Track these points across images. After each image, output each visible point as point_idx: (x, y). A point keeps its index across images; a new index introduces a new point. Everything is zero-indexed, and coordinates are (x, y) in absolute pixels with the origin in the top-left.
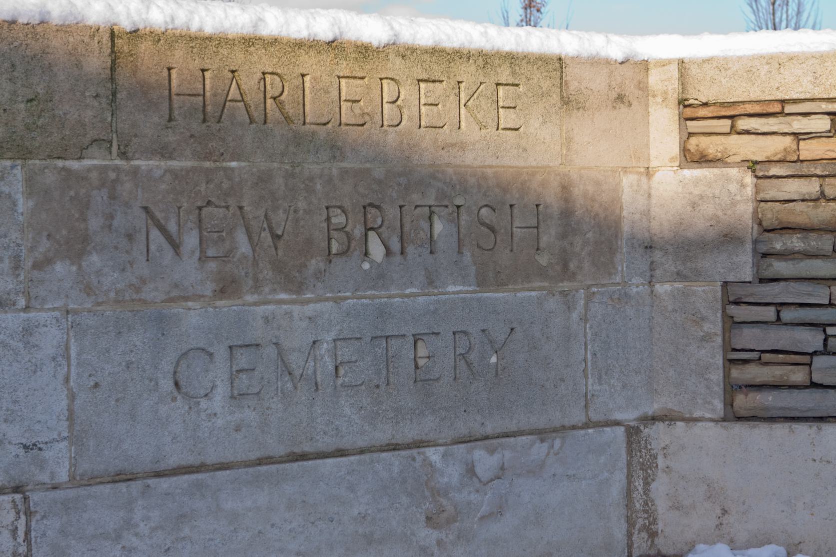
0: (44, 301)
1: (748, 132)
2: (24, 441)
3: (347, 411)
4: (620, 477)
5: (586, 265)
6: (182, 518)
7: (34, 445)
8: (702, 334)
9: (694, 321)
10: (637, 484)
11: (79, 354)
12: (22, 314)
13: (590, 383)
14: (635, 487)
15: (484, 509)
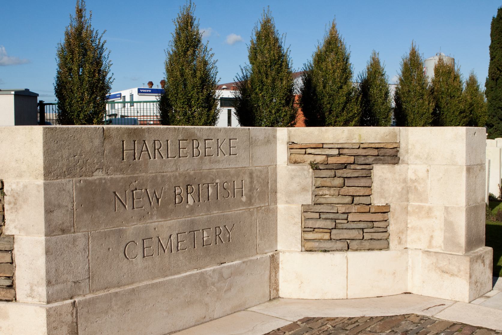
0: (80, 229)
1: (311, 154)
2: (74, 280)
3: (181, 258)
4: (268, 272)
5: (257, 200)
6: (128, 302)
7: (77, 281)
8: (294, 222)
9: (292, 218)
10: (273, 274)
11: (92, 247)
12: (73, 234)
13: (258, 241)
14: (272, 275)
15: (226, 288)
